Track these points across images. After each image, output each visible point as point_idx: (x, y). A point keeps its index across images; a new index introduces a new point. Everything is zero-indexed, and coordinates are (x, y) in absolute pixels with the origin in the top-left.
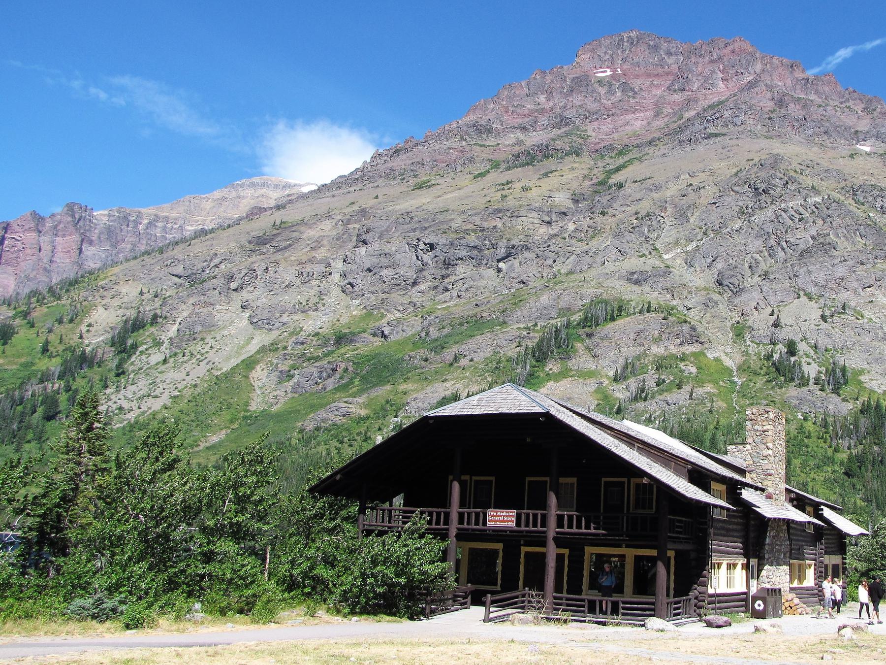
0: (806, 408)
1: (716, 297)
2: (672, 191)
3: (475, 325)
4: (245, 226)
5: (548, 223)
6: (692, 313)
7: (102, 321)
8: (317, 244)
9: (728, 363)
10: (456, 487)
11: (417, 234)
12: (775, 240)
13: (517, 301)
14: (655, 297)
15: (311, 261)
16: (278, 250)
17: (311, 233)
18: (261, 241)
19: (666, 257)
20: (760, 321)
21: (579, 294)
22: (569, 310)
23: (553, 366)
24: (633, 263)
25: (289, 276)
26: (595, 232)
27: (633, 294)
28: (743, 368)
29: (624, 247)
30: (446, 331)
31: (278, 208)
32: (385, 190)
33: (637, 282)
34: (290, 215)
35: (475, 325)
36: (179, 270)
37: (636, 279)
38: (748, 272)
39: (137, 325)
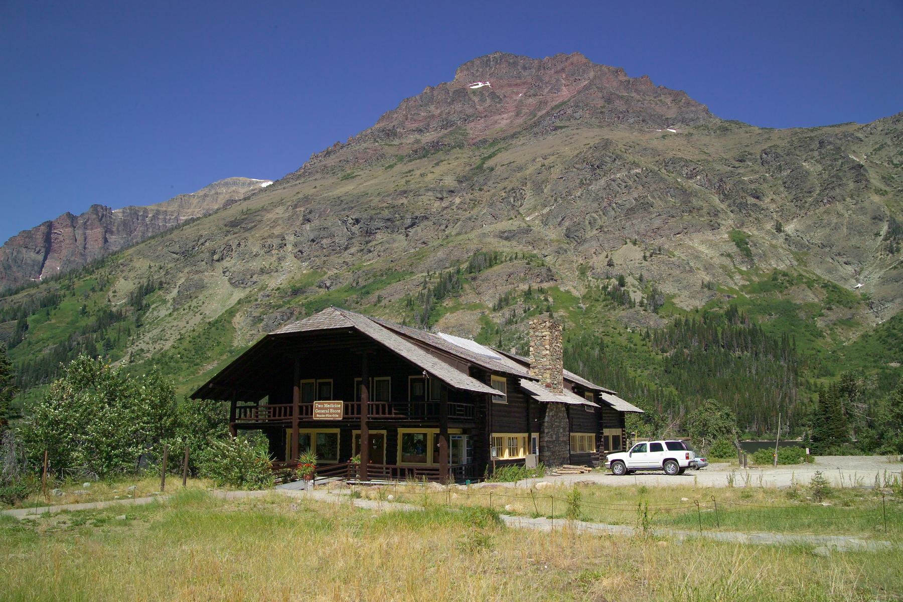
3: (391, 275)
13: (420, 256)
23: (448, 303)
27: (505, 248)
33: (507, 239)
35: (391, 275)
37: (507, 236)
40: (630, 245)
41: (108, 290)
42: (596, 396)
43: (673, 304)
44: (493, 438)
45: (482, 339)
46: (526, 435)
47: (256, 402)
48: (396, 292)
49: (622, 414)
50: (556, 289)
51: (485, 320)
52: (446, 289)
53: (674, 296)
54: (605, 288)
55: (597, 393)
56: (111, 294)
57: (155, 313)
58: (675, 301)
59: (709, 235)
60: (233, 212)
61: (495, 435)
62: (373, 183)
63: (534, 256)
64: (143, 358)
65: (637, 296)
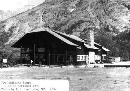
0: (110, 35)
1: (97, 19)
2: (90, 3)
3: (63, 25)
4: (28, 12)
5: (2, 13)
6: (93, 22)
7: (8, 27)
8: (38, 14)
9: (99, 29)
10: (35, 45)
11: (53, 12)
12: (106, 10)
13: (68, 21)
14: (88, 19)
15: (37, 17)
16: (33, 15)
17: (38, 12)
18: (30, 14)
19: (89, 13)
20: (104, 22)
21: (76, 20)
22: (76, 22)
23: (73, 30)
24: (84, 14)
25: (35, 19)
26: (79, 10)
27: (85, 19)
28: (101, 29)
29: (83, 12)
30: (58, 26)
31: (32, 9)
32: (48, 5)
33: (85, 17)
34: (34, 10)
35: (63, 25)
36: (18, 19)
37: (85, 17)
38: (101, 15)
39: (13, 27)
40: (110, 19)
41: (5, 28)
42: (101, 48)
43: (118, 31)
44: (78, 56)
45: (80, 37)
46: (85, 55)
47: (27, 48)
48: (63, 28)
49: (107, 51)
50: (95, 28)
51: (81, 34)
52: (73, 27)
53: (118, 29)
54: (105, 27)
55: (101, 47)
56: (5, 28)
57: (15, 32)
58: (119, 30)
59: (126, 16)
60: (30, 12)
61: (78, 55)
62: (85, 18)
63: (91, 21)
64: (102, 57)
65: (111, 29)
